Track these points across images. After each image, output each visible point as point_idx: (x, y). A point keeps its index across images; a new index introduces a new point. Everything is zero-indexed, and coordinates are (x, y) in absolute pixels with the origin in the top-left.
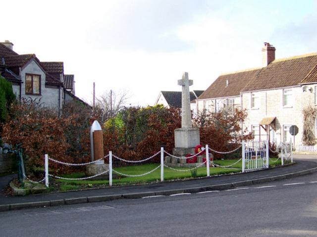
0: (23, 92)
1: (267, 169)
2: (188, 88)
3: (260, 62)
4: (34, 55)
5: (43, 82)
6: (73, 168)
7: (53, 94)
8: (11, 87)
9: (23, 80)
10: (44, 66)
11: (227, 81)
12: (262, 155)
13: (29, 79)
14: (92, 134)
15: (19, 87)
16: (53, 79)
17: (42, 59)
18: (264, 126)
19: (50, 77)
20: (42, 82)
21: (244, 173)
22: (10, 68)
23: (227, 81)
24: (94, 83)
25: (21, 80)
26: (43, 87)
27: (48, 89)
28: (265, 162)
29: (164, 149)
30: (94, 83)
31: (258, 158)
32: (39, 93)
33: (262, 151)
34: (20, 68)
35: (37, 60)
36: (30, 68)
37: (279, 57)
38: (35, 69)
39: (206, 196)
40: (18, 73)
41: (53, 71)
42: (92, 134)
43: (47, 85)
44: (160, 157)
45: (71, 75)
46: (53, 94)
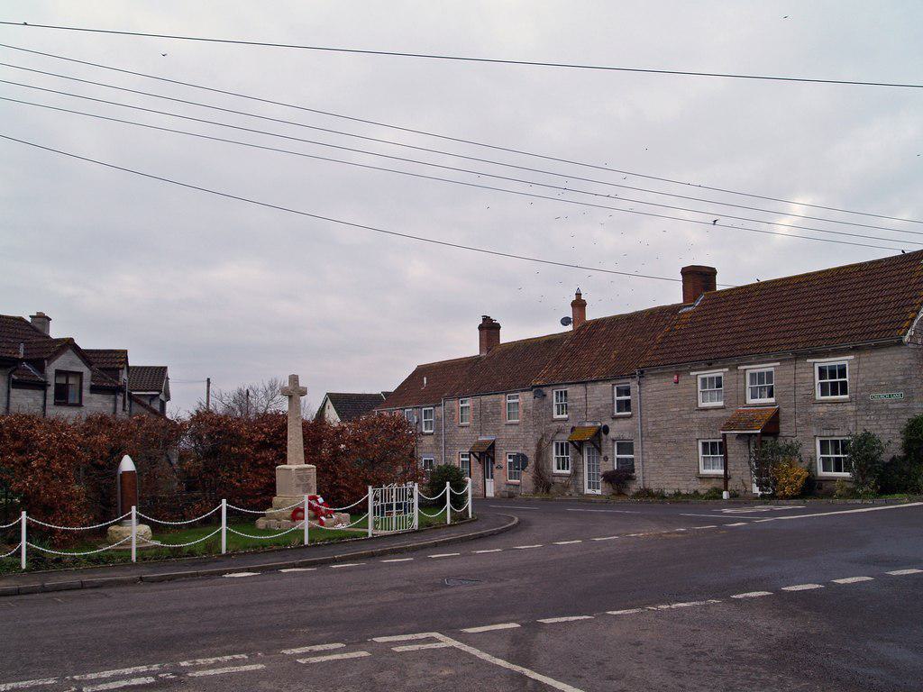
0: (51, 400)
1: (414, 532)
2: (299, 401)
3: (468, 345)
4: (72, 339)
5: (87, 384)
6: (906, 489)
7: (104, 404)
8: (719, 292)
9: (51, 381)
10: (87, 356)
11: (425, 379)
12: (405, 509)
13: (62, 380)
14: (119, 477)
15: (43, 392)
16: (105, 378)
17: (84, 344)
18: (477, 455)
19: (102, 376)
20: (84, 383)
21: (371, 538)
22: (29, 362)
23: (425, 379)
24: (208, 379)
25: (46, 382)
26: (86, 393)
27: (95, 396)
28: (411, 520)
29: (27, 515)
30: (208, 379)
31: (398, 513)
32: (77, 402)
33: (405, 503)
34: (46, 362)
35: (76, 349)
36: (65, 362)
37: (506, 337)
38: (72, 363)
39: (98, 577)
40: (41, 369)
41: (109, 366)
42: (119, 477)
43: (94, 390)
44: (21, 527)
45: (162, 367)
46: (104, 404)
